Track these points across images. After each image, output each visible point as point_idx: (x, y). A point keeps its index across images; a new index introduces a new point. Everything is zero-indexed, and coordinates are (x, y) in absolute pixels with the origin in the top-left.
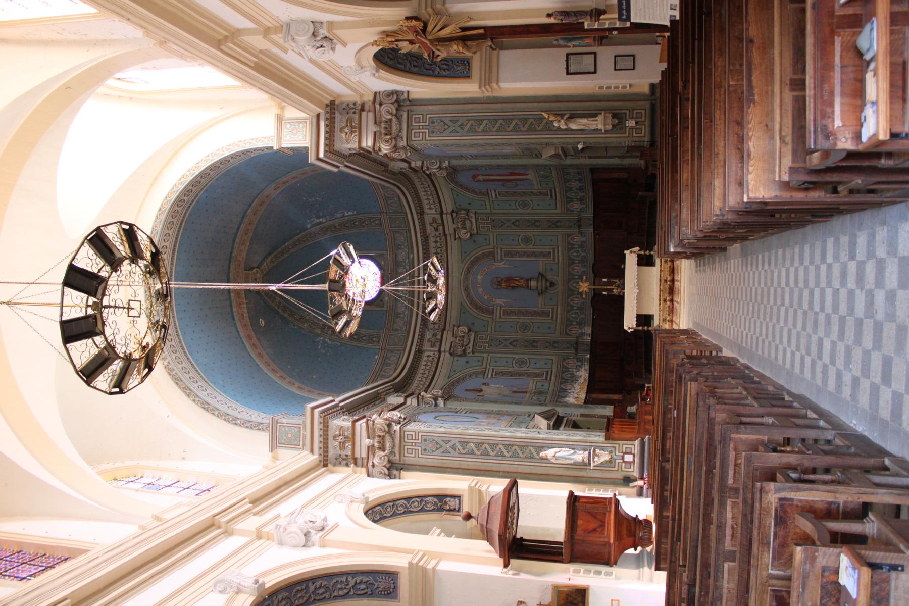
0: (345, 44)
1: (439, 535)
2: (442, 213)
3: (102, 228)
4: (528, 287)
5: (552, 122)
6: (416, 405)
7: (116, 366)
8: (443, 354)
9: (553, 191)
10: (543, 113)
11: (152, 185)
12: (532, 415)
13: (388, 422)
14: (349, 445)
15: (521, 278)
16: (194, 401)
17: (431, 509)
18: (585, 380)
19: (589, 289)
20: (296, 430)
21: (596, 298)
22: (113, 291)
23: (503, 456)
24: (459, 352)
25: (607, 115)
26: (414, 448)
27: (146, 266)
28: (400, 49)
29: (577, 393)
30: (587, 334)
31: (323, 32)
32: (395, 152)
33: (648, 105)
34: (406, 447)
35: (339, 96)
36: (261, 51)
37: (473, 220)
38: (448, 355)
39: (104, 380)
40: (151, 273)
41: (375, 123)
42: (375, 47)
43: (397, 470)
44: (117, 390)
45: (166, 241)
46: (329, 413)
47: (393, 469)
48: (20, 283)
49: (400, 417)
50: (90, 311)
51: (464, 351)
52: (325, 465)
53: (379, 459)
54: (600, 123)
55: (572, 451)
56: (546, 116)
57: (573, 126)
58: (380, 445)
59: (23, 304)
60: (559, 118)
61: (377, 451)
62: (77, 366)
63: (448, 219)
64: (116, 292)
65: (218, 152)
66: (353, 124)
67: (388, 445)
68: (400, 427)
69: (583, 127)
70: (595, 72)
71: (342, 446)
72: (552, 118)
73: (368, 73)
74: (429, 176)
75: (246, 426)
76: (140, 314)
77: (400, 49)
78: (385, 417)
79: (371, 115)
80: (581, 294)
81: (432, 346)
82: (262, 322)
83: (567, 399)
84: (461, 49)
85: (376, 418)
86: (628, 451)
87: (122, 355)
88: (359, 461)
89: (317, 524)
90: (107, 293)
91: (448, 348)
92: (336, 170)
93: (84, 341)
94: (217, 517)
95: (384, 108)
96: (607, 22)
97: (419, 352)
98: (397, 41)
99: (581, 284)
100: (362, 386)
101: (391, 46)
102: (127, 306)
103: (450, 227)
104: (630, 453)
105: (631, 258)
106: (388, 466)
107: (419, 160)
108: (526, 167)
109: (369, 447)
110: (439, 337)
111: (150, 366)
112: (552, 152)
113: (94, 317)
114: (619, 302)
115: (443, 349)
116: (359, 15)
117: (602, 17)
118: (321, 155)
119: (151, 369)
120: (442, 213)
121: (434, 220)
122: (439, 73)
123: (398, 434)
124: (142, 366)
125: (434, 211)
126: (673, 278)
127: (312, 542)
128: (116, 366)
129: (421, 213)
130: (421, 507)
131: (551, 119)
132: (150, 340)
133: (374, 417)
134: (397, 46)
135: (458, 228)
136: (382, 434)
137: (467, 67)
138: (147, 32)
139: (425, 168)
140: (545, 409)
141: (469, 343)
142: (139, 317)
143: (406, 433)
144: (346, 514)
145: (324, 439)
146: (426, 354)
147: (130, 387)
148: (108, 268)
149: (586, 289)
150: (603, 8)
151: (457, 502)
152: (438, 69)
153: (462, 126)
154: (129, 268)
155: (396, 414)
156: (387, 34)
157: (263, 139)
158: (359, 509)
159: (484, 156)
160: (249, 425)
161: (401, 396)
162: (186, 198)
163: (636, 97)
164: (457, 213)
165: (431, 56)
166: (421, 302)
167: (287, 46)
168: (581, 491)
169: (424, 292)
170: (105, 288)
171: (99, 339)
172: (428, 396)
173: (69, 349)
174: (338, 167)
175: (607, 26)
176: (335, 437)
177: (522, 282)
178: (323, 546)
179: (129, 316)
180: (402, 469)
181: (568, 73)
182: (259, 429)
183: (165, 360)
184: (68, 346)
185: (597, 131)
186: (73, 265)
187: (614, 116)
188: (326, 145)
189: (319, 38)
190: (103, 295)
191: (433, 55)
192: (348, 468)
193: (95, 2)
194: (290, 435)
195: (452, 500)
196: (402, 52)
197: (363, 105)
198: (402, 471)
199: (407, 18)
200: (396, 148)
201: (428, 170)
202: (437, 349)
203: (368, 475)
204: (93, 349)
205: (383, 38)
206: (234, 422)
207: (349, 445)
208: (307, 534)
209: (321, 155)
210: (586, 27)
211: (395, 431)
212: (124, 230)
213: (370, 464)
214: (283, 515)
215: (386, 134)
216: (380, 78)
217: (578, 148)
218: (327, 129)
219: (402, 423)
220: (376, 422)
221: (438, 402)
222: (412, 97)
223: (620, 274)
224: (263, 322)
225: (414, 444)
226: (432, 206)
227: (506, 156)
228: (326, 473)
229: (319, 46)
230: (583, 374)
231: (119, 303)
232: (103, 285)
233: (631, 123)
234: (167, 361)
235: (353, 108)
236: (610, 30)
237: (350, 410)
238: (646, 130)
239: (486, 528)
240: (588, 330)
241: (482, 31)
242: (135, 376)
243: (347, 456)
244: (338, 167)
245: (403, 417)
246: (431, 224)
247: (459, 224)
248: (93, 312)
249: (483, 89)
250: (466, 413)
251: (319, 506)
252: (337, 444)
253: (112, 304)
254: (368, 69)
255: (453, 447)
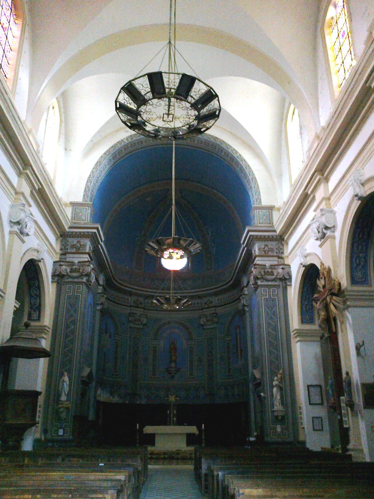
0: (321, 246)
1: (15, 306)
2: (215, 307)
3: (217, 98)
4: (171, 362)
5: (277, 376)
6: (98, 292)
7: (133, 106)
8: (129, 308)
9: (232, 377)
10: (282, 370)
11: (231, 133)
12: (90, 366)
13: (88, 274)
14: (74, 250)
15: (176, 357)
16: (102, 157)
17: (32, 302)
18: (112, 400)
19: (171, 402)
20: (84, 218)
21: (165, 407)
22: (180, 104)
23: (65, 348)
24: (130, 319)
25: (283, 413)
26: (271, 293)
27: (193, 125)
28: (319, 280)
29: (103, 396)
30: (141, 401)
31: (328, 233)
32: (254, 277)
33: (291, 439)
34: (81, 286)
35: (287, 244)
36: (314, 197)
37: (212, 326)
38: (129, 311)
39: (124, 98)
40: (190, 127)
41: (271, 265)
42: (320, 264)
43: (58, 280)
44: (118, 106)
45: (198, 142)
46: (93, 238)
47: (58, 277)
48: (45, 132)
49: (91, 282)
50: (167, 90)
51: (131, 322)
52: (61, 236)
53: (65, 269)
54: (278, 407)
55: (66, 393)
56: (281, 372)
57: (275, 390)
58: (74, 270)
59: (170, 51)
60: (279, 380)
61: (70, 267)
62: (134, 82)
63: (212, 310)
64: (179, 107)
65: (251, 172)
66: (270, 252)
67: (74, 274)
68: (85, 282)
69: (275, 396)
70: (310, 404)
71: (73, 246)
72: (279, 376)
73: (302, 260)
74: (239, 299)
75: (87, 188)
76: (165, 121)
77: (319, 280)
78: (92, 273)
79: (276, 263)
80: (168, 397)
81: (134, 302)
82: (148, 199)
83: (100, 389)
84: (322, 317)
85: (91, 267)
86: (66, 432)
87: (140, 109)
88: (64, 257)
89: (25, 229)
90: (178, 100)
91: (132, 311)
92: (242, 242)
93: (149, 87)
94: (30, 168)
95: (280, 270)
96: (345, 412)
97: (130, 294)
98: (325, 277)
99: (174, 396)
100: (110, 259)
101: (321, 274)
102: (170, 113)
103: (208, 312)
104: (64, 433)
105: (193, 429)
106: (61, 274)
107: (248, 293)
108: (246, 360)
109: (72, 262)
110: (140, 306)
111: (132, 127)
112: (258, 375)
113: (164, 92)
114: (164, 422)
115: (133, 308)
116: (340, 254)
117: (349, 409)
118: (250, 233)
119: (130, 127)
120: (215, 307)
121: (212, 302)
122: (304, 304)
123: (80, 280)
124: (133, 122)
125: (217, 301)
126: (180, 459)
127: (13, 226)
128: (133, 106)
129: (216, 294)
130: (33, 295)
131: (278, 375)
132: (149, 128)
133: (92, 266)
134: (322, 278)
135: (207, 317)
136: (81, 271)
137: (308, 321)
138: (324, 129)
139: (243, 296)
140: (94, 374)
141: (136, 324)
142: (163, 121)
143: (81, 286)
144: (30, 249)
145: (70, 235)
146: (130, 298)
147: (120, 114)
148: (193, 101)
149: (170, 400)
150: (355, 409)
151: (36, 318)
152: (306, 303)
153: (271, 318)
154: (193, 114)
155: (93, 280)
156: (329, 271)
157: (259, 199)
158: (35, 256)
159: (252, 333)
160: (87, 190)
161: (104, 282)
162: (223, 153)
163: (296, 432)
164: (216, 316)
165: (316, 299)
166: (162, 295)
167: (319, 211)
168: (41, 400)
169: (170, 296)
170: (181, 100)
171: (150, 95)
172: (103, 300)
173: (144, 77)
174: (243, 243)
175: (343, 411)
176: (78, 242)
177: (174, 358)
178: (11, 233)
179: (164, 114)
180: (58, 283)
181: (308, 386)
182: (84, 195)
183: (126, 140)
184: (147, 76)
185: (273, 405)
186: (195, 81)
187: (283, 417)
188: (257, 236)
189: (324, 230)
190: (177, 99)
191: (316, 300)
192: (59, 249)
193: (366, 91)
194: (80, 214)
195: (37, 315)
196: (318, 281)
197: (282, 258)
198: (56, 283)
199: (340, 284)
200: (256, 278)
201: (242, 298)
202: (132, 304)
203: (54, 262)
204: (144, 91)
205: (326, 269)
206: (89, 181)
207: (74, 250)
208: (18, 223)
209: (250, 233)
210: (341, 398)
211: (83, 279)
212: (215, 112)
213: (62, 263)
214: (30, 209)
215: (264, 272)
216: (299, 268)
217: (261, 393)
218: (267, 237)
219: (87, 283)
220: (89, 267)
221: (100, 306)
222: (288, 288)
223: (180, 423)
224: (148, 200)
225: (74, 290)
226: (220, 301)
227: (252, 346)
228: (56, 236)
229: (319, 230)
230: (116, 399)
231: (172, 108)
232: (183, 98)
233: (279, 429)
234: (126, 141)
235: (279, 252)
236: (340, 414)
237: (96, 251)
238: (274, 438)
239: (19, 337)
240: (144, 402)
241: (334, 330)
242: (126, 117)
243: (67, 249)
244: (243, 243)
245: (92, 284)
246: (209, 300)
247: (209, 317)
248: (167, 92)
249: (295, 332)
250: (93, 323)
251: (36, 232)
252: (75, 243)
253: (171, 104)
254: (305, 261)
255: (72, 316)
